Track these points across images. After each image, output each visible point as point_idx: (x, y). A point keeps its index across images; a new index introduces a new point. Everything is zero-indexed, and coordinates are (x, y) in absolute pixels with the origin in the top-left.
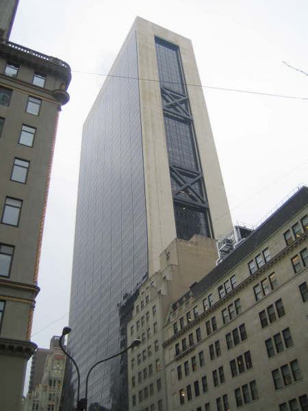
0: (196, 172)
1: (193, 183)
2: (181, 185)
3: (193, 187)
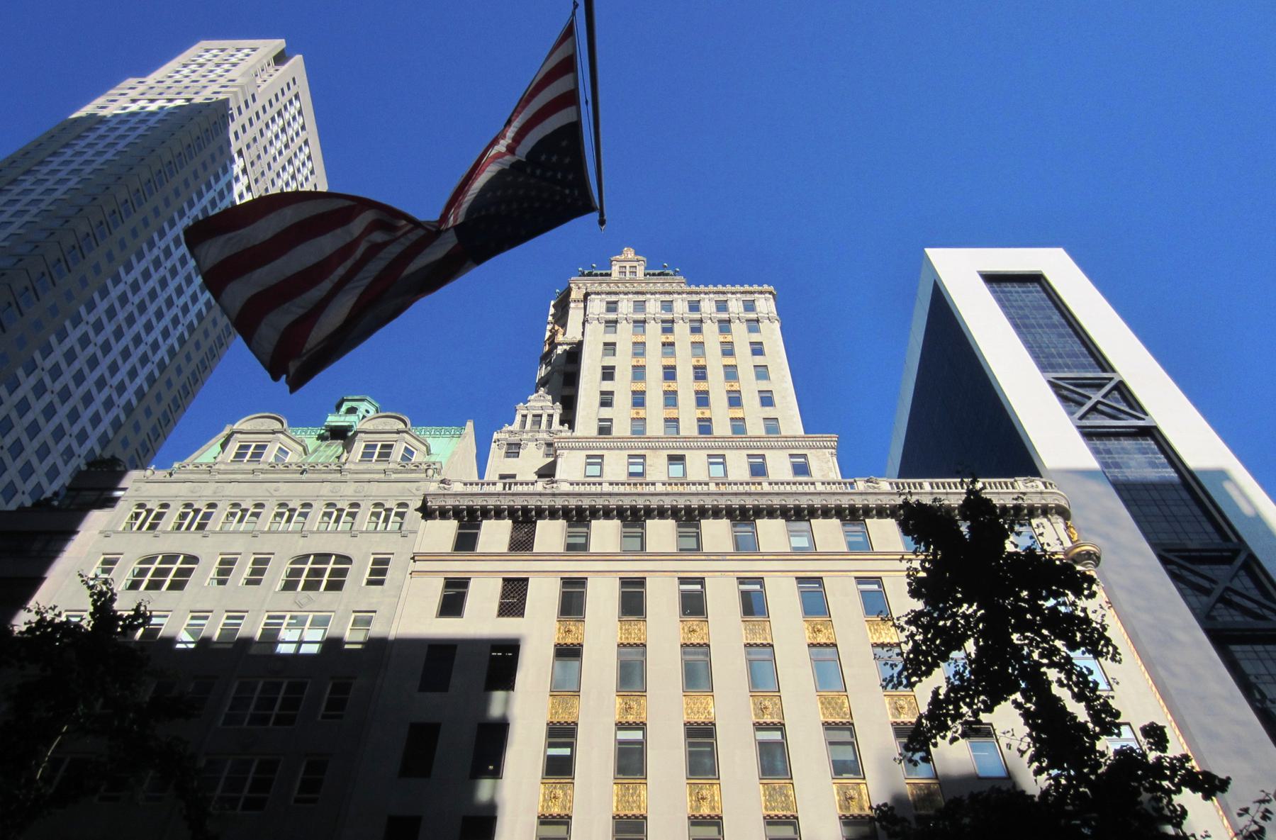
0: (1229, 545)
1: (1236, 575)
2: (1207, 592)
3: (1237, 585)
